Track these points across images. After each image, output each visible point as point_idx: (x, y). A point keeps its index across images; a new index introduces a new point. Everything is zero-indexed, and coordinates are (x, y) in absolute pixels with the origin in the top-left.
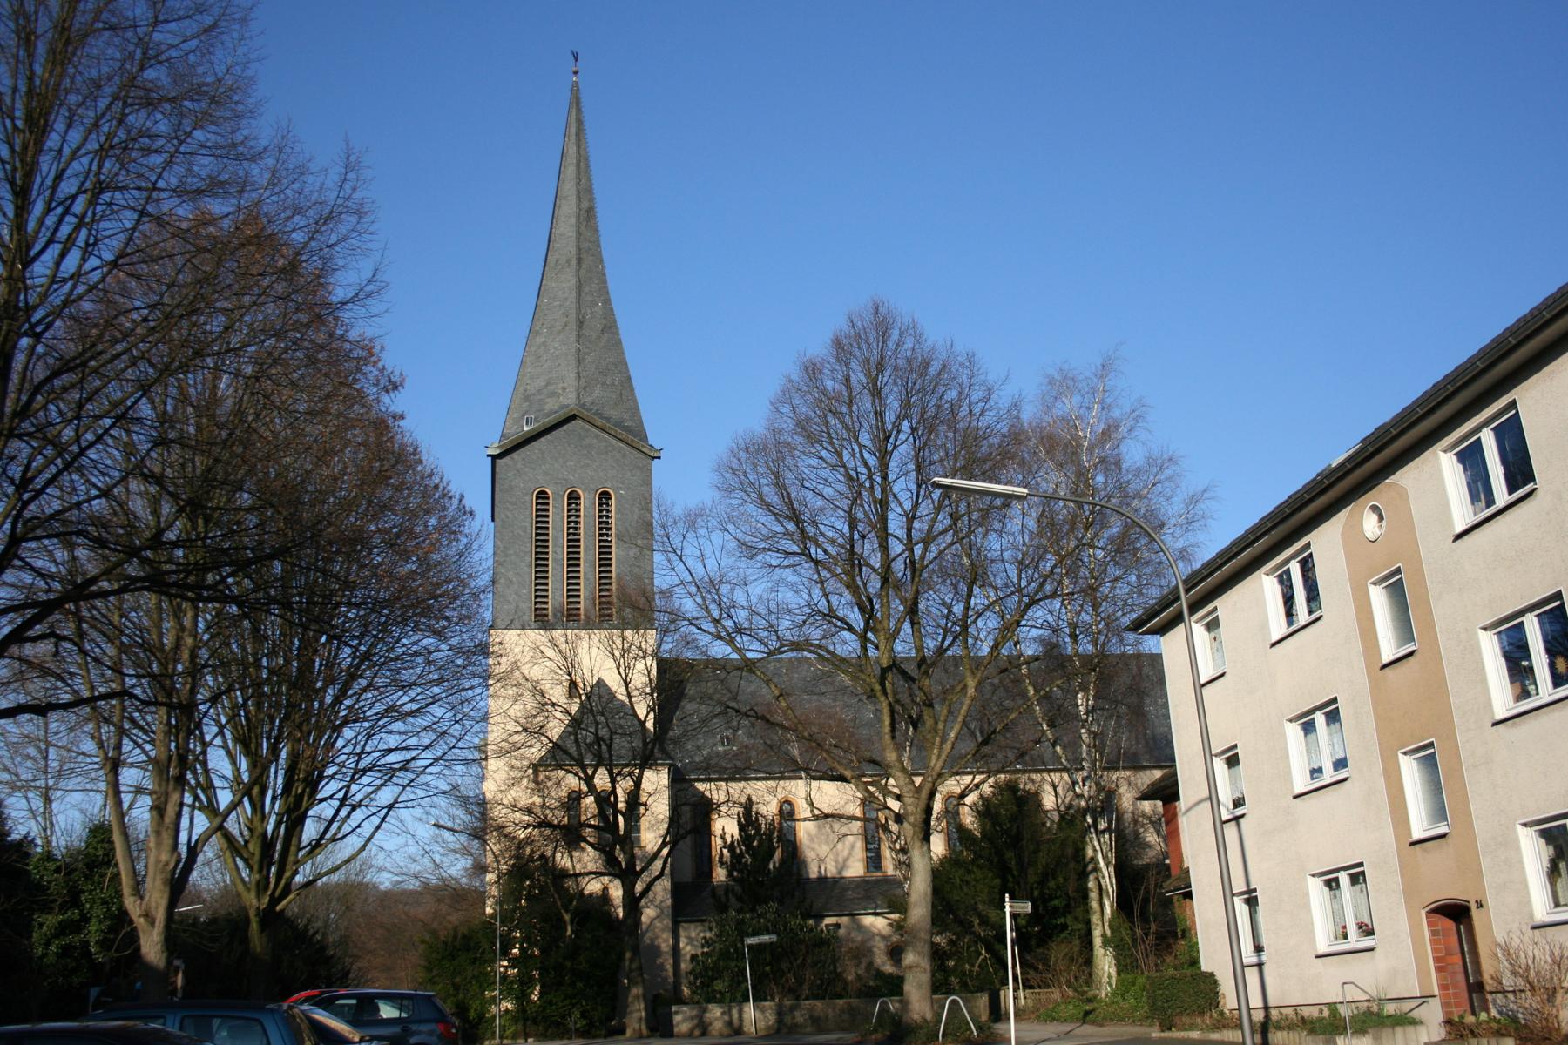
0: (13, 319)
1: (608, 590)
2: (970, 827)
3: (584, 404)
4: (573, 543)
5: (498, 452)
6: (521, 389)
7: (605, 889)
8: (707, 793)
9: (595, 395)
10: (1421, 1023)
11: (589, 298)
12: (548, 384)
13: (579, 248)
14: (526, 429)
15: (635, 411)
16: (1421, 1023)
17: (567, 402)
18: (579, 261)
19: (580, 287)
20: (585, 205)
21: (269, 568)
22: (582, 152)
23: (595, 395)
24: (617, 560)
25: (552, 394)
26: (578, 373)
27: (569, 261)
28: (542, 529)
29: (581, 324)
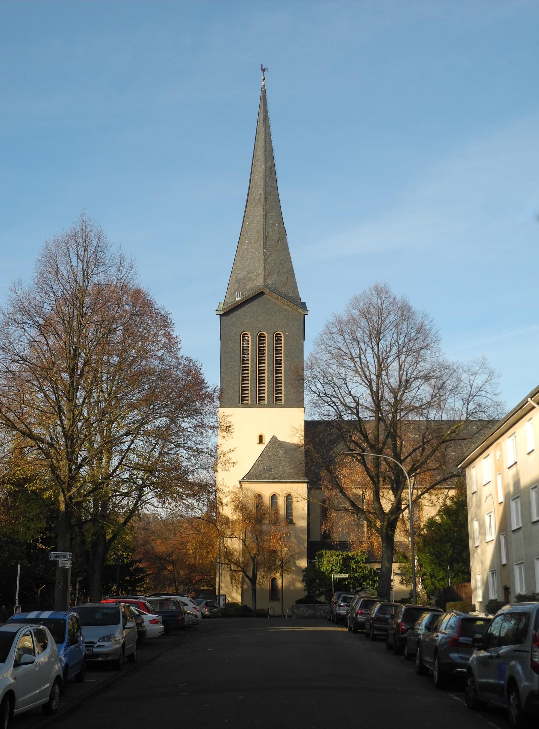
0: (176, 502)
1: (280, 370)
2: (476, 623)
3: (267, 285)
4: (261, 371)
5: (222, 313)
6: (234, 277)
7: (479, 602)
8: (399, 519)
9: (273, 279)
10: (188, 605)
11: (271, 222)
12: (248, 273)
13: (265, 191)
14: (237, 299)
15: (295, 287)
16: (188, 605)
17: (259, 284)
18: (266, 199)
19: (265, 215)
20: (269, 164)
21: (94, 366)
22: (267, 131)
23: (273, 279)
24: (285, 370)
25: (251, 279)
26: (265, 267)
27: (260, 199)
28: (244, 363)
29: (266, 238)
